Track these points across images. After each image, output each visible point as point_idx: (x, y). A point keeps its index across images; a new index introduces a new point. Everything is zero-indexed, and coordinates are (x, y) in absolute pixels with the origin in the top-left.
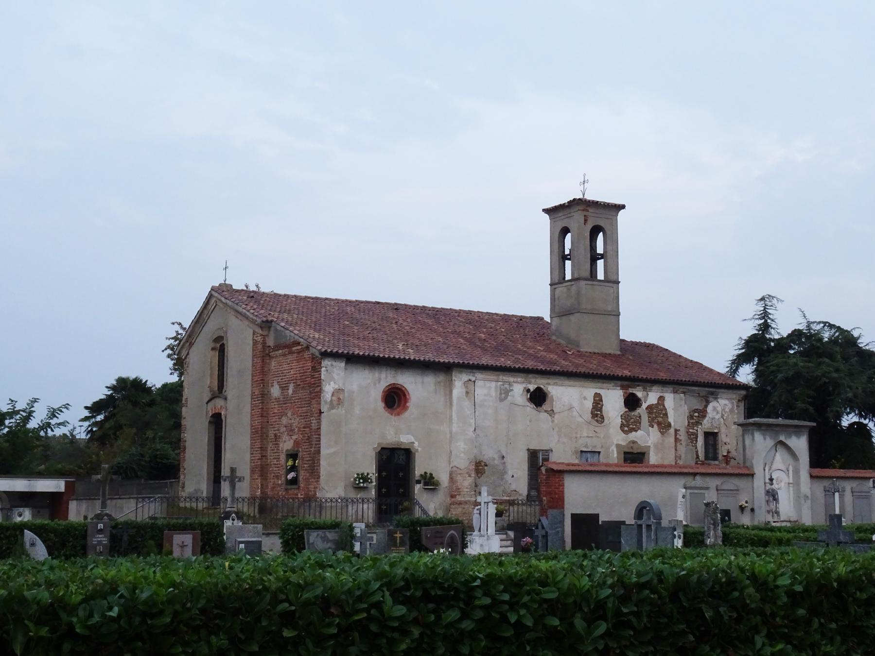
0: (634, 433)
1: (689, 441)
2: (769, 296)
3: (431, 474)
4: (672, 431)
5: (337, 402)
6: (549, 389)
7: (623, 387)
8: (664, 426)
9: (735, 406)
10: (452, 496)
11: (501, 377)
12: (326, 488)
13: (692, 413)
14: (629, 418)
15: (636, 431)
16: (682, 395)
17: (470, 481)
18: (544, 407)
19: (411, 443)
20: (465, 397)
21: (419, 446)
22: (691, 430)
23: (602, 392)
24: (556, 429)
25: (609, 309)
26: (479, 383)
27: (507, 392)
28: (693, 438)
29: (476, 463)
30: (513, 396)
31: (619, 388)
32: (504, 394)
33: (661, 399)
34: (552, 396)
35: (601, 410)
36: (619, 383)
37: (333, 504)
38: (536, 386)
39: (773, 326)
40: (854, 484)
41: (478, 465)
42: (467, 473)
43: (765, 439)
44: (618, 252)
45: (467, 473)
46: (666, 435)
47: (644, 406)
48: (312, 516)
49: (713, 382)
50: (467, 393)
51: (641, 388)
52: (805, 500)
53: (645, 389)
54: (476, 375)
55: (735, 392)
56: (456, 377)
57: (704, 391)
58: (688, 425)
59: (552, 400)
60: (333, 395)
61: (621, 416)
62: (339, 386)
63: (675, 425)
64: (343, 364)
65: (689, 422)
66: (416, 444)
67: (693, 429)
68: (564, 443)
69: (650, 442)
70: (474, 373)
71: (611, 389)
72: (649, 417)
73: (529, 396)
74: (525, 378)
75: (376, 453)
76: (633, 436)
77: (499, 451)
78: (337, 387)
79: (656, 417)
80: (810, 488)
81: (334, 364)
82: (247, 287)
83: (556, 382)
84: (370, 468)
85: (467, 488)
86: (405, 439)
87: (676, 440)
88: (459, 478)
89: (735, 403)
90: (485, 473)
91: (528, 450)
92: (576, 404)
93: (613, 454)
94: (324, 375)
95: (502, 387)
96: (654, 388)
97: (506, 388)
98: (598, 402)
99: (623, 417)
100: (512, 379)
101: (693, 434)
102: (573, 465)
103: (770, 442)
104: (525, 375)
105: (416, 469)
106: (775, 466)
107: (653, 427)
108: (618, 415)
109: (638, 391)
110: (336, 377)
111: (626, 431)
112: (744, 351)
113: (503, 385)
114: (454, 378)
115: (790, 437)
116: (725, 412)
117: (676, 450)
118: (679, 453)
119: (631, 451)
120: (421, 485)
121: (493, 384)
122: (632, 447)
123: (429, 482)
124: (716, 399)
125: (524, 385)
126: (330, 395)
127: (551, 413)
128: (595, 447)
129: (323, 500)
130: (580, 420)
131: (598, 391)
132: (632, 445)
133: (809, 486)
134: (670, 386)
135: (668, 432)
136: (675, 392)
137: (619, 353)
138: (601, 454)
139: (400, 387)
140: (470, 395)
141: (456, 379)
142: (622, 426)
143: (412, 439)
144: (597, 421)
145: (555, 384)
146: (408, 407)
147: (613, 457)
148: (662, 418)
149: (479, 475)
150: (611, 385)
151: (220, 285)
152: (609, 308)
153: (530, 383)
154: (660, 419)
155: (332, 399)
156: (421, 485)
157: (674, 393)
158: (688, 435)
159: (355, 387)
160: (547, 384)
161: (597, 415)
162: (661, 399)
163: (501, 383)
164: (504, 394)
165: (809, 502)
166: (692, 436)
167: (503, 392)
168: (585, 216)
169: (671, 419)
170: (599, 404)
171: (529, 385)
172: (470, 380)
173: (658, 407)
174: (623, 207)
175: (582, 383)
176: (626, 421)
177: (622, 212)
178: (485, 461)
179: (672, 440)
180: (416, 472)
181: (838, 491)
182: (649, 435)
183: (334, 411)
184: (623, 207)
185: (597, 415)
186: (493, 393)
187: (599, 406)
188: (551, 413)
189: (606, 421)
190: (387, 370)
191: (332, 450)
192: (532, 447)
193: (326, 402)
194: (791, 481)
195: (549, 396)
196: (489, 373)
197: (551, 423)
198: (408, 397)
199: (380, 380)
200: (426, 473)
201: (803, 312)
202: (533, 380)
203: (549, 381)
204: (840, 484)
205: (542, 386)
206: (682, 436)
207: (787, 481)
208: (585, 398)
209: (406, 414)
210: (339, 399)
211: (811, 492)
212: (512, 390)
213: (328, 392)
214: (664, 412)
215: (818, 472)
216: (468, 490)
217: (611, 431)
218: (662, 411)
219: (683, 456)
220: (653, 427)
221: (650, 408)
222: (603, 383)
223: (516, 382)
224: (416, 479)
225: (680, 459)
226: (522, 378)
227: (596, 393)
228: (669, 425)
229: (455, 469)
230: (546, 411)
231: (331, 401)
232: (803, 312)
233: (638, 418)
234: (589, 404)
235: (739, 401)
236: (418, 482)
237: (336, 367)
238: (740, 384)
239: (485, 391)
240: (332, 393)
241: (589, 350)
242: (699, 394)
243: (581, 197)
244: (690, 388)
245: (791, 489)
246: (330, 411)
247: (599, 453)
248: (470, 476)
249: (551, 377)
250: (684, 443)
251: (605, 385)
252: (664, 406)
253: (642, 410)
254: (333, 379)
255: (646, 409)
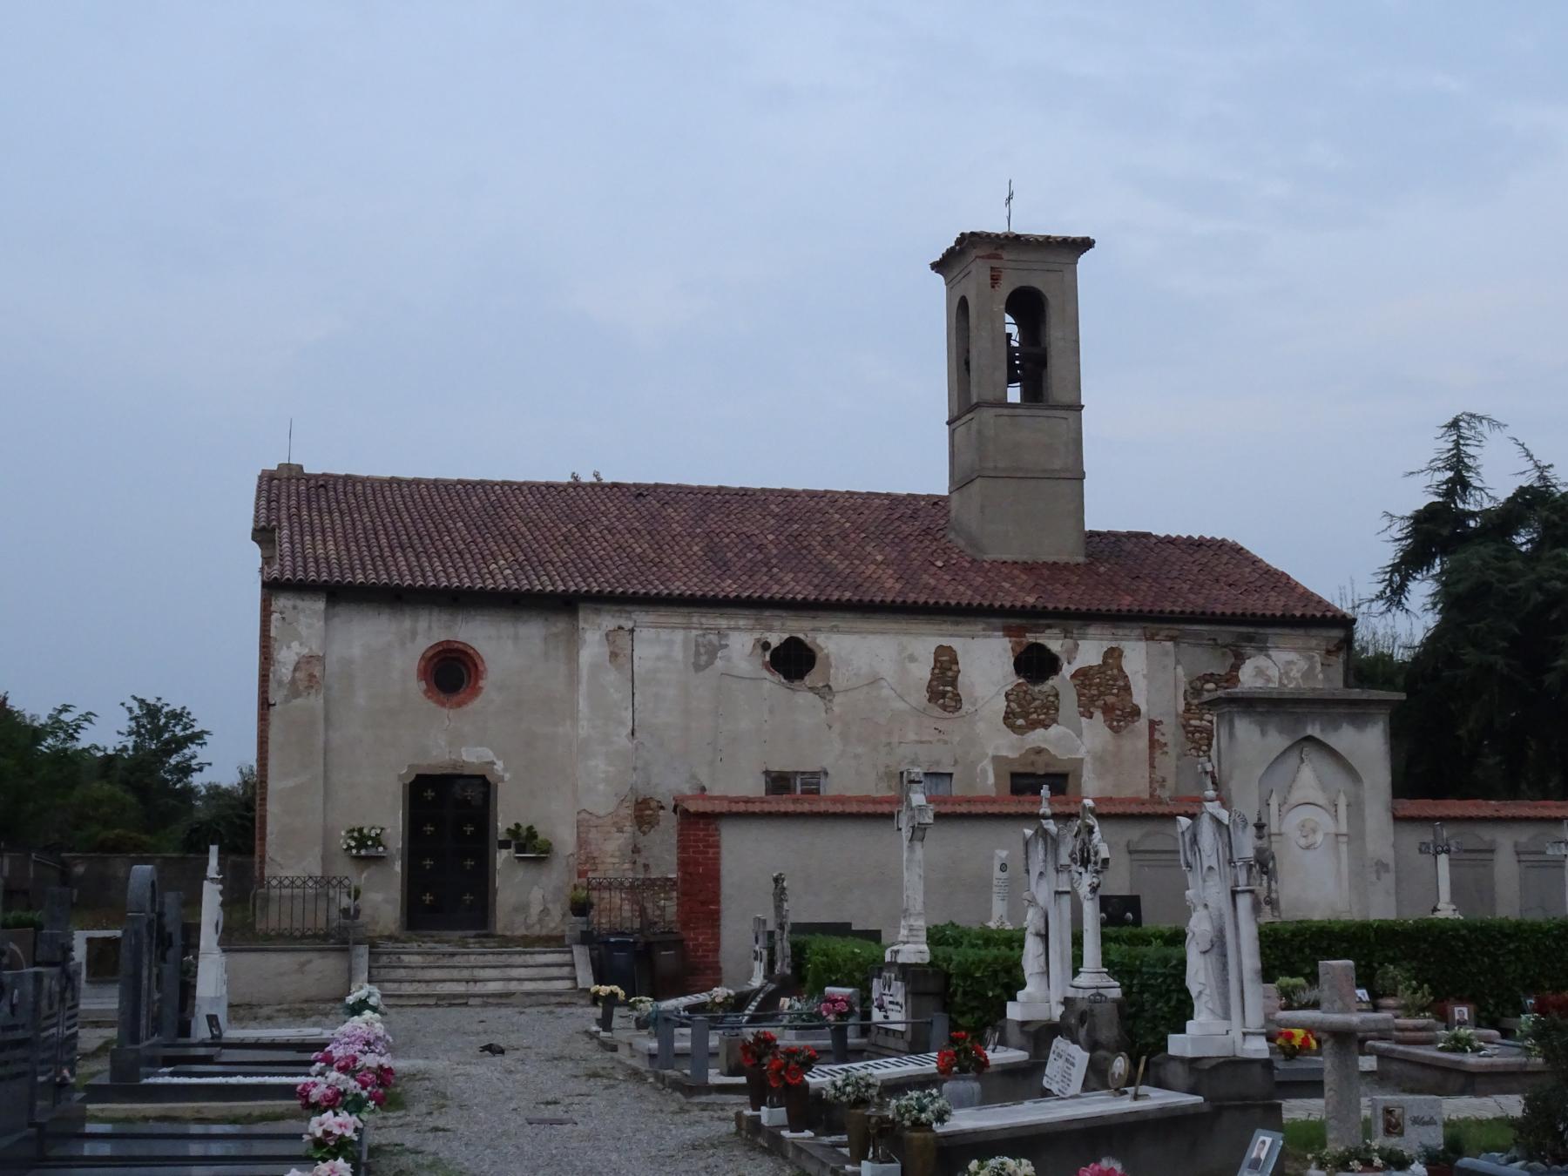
0: (1040, 731)
1: (1190, 746)
2: (1473, 416)
3: (530, 828)
4: (1142, 724)
5: (306, 683)
6: (818, 641)
7: (1008, 631)
8: (1121, 714)
9: (1319, 667)
10: (581, 874)
11: (695, 620)
12: (278, 859)
13: (1199, 684)
14: (1028, 697)
15: (1046, 727)
16: (1169, 644)
17: (620, 842)
18: (809, 680)
19: (488, 763)
20: (608, 664)
21: (505, 770)
22: (1193, 722)
23: (956, 643)
24: (837, 727)
25: (1057, 467)
26: (643, 634)
27: (713, 652)
28: (1201, 739)
29: (637, 803)
30: (728, 659)
31: (1001, 633)
32: (705, 656)
33: (1113, 655)
34: (827, 657)
35: (953, 682)
36: (997, 622)
37: (296, 891)
38: (786, 636)
39: (1476, 483)
40: (1524, 835)
41: (642, 806)
42: (615, 824)
43: (1263, 733)
44: (1077, 342)
45: (615, 824)
46: (1124, 732)
47: (1067, 670)
48: (920, 933)
49: (1249, 612)
50: (614, 655)
51: (1056, 631)
52: (1378, 872)
53: (1067, 634)
54: (634, 616)
55: (1314, 632)
56: (585, 621)
57: (1226, 633)
58: (1187, 710)
59: (829, 666)
60: (295, 669)
61: (1007, 695)
62: (311, 649)
63: (1148, 710)
64: (320, 605)
65: (1188, 704)
66: (499, 766)
67: (1201, 719)
68: (857, 756)
69: (1083, 750)
70: (630, 612)
71: (978, 636)
72: (1079, 695)
73: (768, 658)
74: (757, 620)
75: (404, 785)
76: (1037, 737)
77: (693, 777)
78: (305, 651)
79: (1101, 694)
80: (1394, 846)
81: (300, 604)
82: (576, 478)
83: (835, 626)
84: (391, 823)
85: (612, 856)
86: (472, 756)
87: (1153, 744)
88: (593, 834)
89: (1318, 658)
90: (658, 824)
91: (767, 773)
92: (887, 669)
93: (986, 778)
94: (276, 627)
95: (700, 640)
96: (1091, 631)
97: (710, 643)
98: (946, 667)
99: (1011, 697)
100: (723, 623)
101: (1198, 729)
102: (875, 801)
103: (1277, 741)
104: (753, 612)
105: (500, 818)
106: (1297, 796)
107: (1091, 717)
108: (998, 693)
109: (1049, 638)
110: (304, 632)
111: (1020, 727)
112: (1409, 541)
113: (704, 635)
114: (581, 624)
115: (1336, 728)
116: (1288, 677)
117: (1152, 766)
118: (1159, 774)
119: (1030, 770)
120: (512, 850)
121: (679, 636)
122: (1033, 764)
123: (531, 847)
124: (1263, 650)
125: (757, 635)
126: (291, 668)
127: (825, 692)
128: (938, 763)
129: (274, 883)
130: (900, 705)
131: (946, 642)
132: (1033, 757)
133: (1392, 838)
134: (1134, 625)
135: (1131, 726)
136: (1150, 638)
137: (1081, 559)
138: (954, 776)
139: (461, 646)
140: (621, 660)
141: (586, 626)
142: (1009, 718)
143: (486, 754)
144: (944, 708)
145: (834, 630)
146: (481, 688)
147: (988, 781)
148: (1117, 695)
149: (645, 828)
150: (980, 627)
151: (280, 466)
152: (1057, 464)
153: (770, 629)
154: (1111, 699)
155: (293, 677)
156: (512, 850)
157: (1147, 639)
158: (1188, 732)
159: (356, 651)
160: (813, 630)
161: (943, 695)
162: (1113, 655)
163: (700, 632)
164: (705, 656)
165: (1389, 879)
166: (1197, 735)
167: (702, 650)
168: (992, 269)
169: (1140, 698)
170: (950, 669)
171: (767, 635)
172: (621, 628)
173: (1104, 673)
174: (1086, 244)
175: (904, 626)
176: (1020, 705)
177: (1085, 261)
178: (658, 798)
179: (1143, 743)
180: (499, 824)
181: (1448, 852)
182: (1079, 735)
183: (298, 702)
184: (1086, 244)
185: (943, 695)
186: (678, 653)
187: (950, 674)
188: (825, 692)
189: (966, 707)
190: (430, 614)
191: (291, 783)
192: (776, 767)
193: (280, 683)
194: (1344, 829)
195: (819, 655)
196: (663, 611)
197: (823, 715)
198: (481, 668)
199: (414, 634)
200: (518, 825)
201: (1523, 445)
202: (777, 624)
203: (817, 624)
204: (1487, 834)
205: (801, 636)
206: (1170, 733)
207: (1332, 829)
208: (912, 659)
209: (476, 704)
210: (311, 676)
211: (1396, 852)
212: (727, 646)
213: (285, 664)
214: (1121, 683)
215: (1412, 807)
216: (616, 860)
217: (981, 727)
218: (1116, 680)
219: (1171, 782)
220: (1091, 717)
221: (1083, 675)
222: (957, 623)
223: (734, 628)
224: (500, 839)
225: (1162, 786)
226: (748, 619)
227: (941, 647)
228: (1136, 712)
229: (584, 815)
230: (811, 689)
231: (293, 681)
232: (1523, 445)
233: (1051, 699)
234: (923, 671)
235: (1329, 652)
236: (505, 845)
237: (303, 610)
238: (1334, 616)
239: (658, 650)
240: (294, 663)
241: (1005, 557)
242: (1215, 640)
243: (1006, 230)
244: (1181, 627)
245: (1344, 848)
246: (290, 701)
247: (950, 775)
248: (620, 830)
249: (820, 613)
250: (1173, 751)
251: (963, 629)
252: (1121, 670)
253: (1062, 681)
254: (297, 636)
255: (1073, 676)
